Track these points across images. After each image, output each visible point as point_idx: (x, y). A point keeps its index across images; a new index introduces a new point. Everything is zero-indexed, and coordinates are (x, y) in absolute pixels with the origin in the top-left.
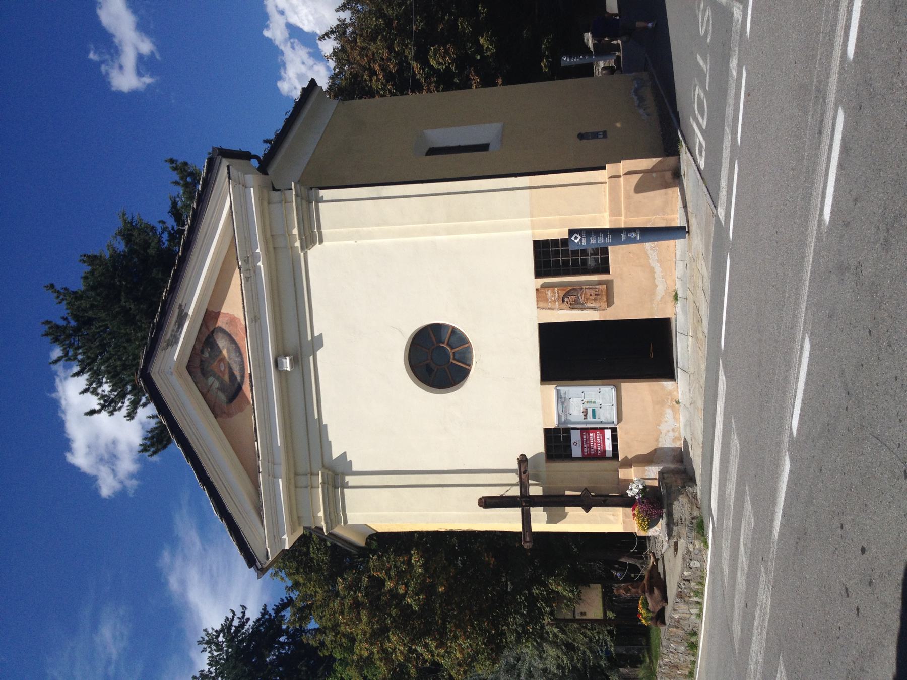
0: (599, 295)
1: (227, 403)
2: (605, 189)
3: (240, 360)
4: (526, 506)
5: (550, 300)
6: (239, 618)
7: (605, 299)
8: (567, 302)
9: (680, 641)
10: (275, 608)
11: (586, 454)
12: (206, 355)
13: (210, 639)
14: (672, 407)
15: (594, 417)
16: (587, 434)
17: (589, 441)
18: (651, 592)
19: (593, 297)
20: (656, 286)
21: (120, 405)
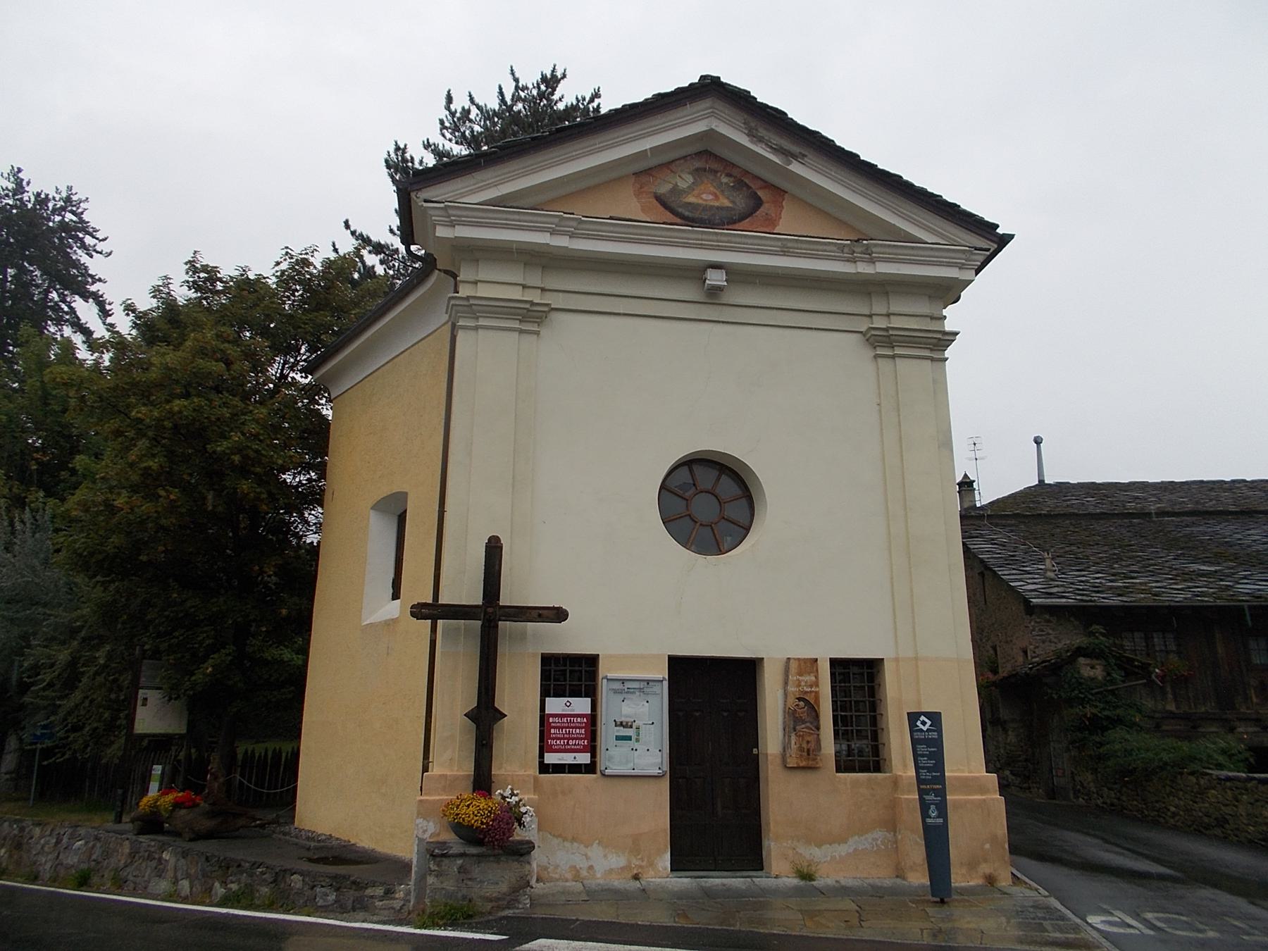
0: (808, 754)
1: (655, 193)
3: (717, 221)
4: (486, 613)
5: (801, 678)
6: (95, 246)
7: (801, 765)
8: (797, 705)
9: (94, 857)
10: (100, 293)
11: (551, 720)
12: (725, 180)
13: (71, 202)
16: (584, 725)
17: (573, 728)
18: (211, 815)
19: (805, 745)
21: (448, 136)
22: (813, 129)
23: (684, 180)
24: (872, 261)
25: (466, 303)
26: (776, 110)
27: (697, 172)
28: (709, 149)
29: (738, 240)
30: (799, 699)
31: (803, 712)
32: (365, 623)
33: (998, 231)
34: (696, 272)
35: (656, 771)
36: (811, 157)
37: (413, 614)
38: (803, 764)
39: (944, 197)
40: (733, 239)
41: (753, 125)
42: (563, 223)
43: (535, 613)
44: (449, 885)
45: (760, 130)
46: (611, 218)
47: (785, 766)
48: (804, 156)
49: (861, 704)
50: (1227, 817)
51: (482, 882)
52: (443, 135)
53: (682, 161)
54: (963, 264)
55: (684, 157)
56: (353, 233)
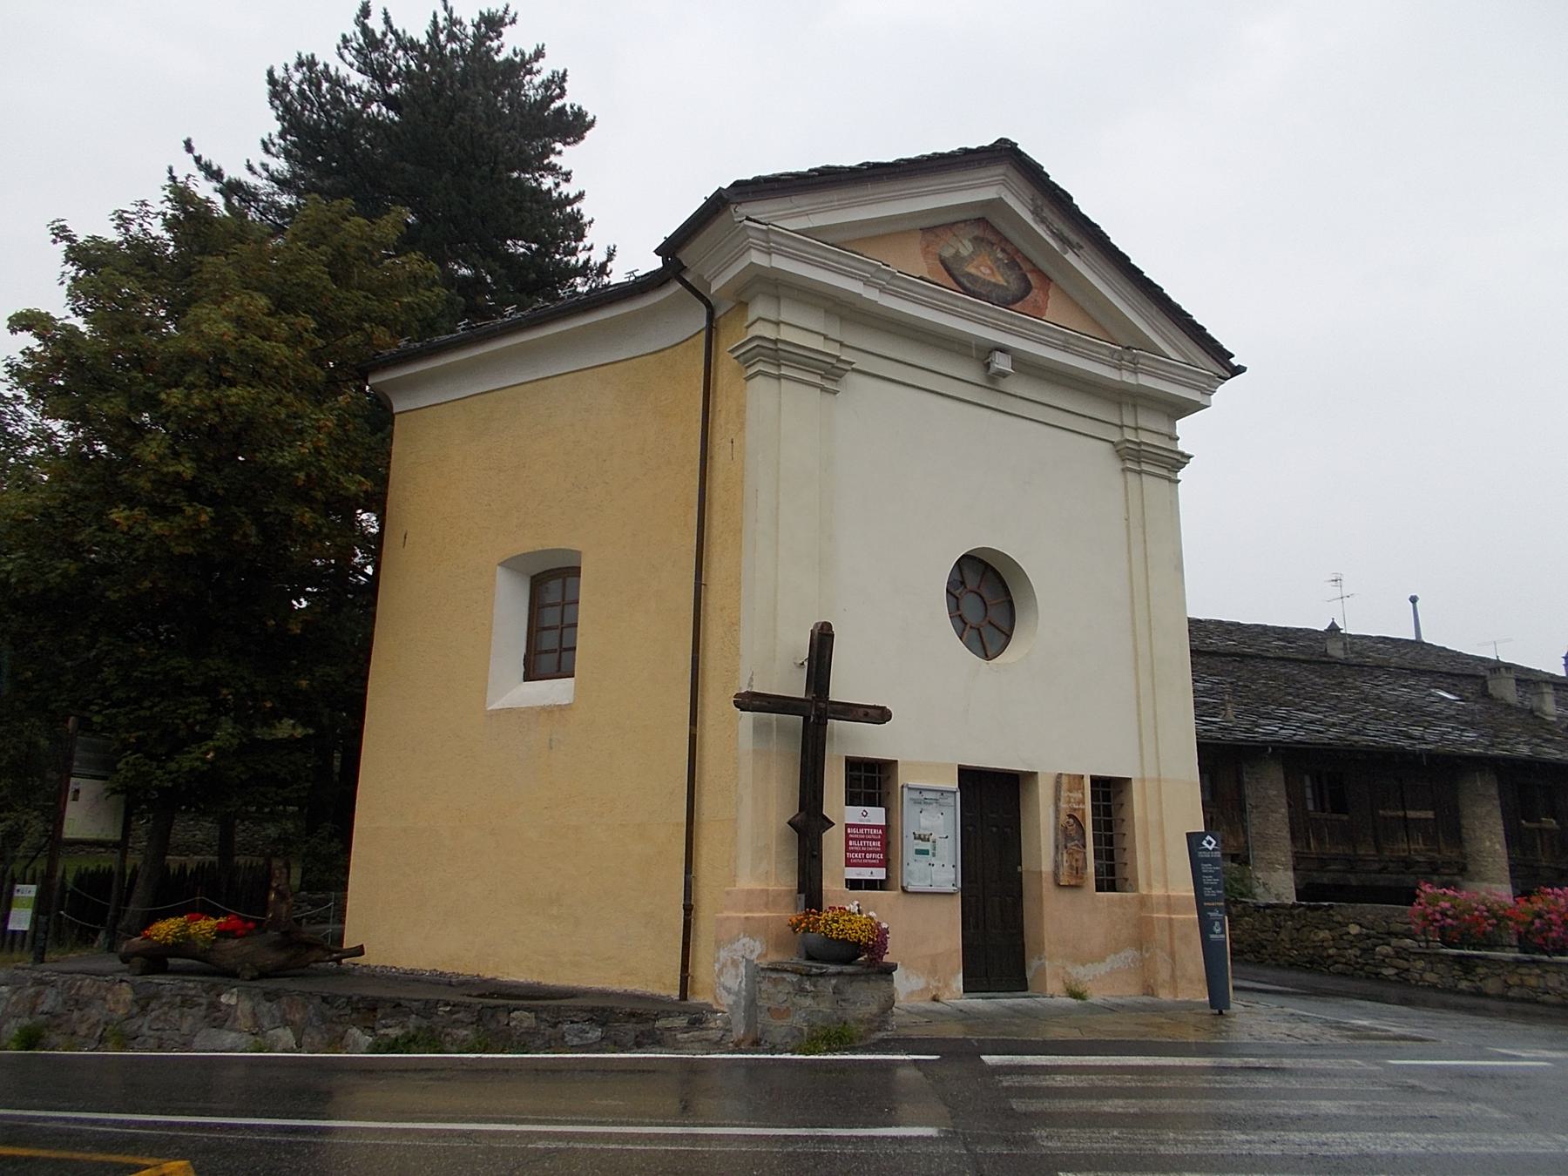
2: (1188, 891)
12: (1000, 255)
14: (926, 989)
15: (919, 852)
17: (869, 840)
19: (1074, 863)
20: (1083, 965)
21: (350, 58)
22: (1095, 222)
23: (966, 249)
24: (1135, 372)
25: (771, 346)
26: (1065, 192)
27: (977, 241)
28: (987, 218)
29: (1029, 326)
30: (1070, 816)
31: (1072, 830)
32: (496, 706)
33: (1231, 360)
34: (984, 353)
35: (951, 889)
36: (1088, 250)
37: (737, 704)
38: (1073, 883)
39: (1194, 318)
40: (1025, 325)
41: (1039, 203)
42: (877, 274)
43: (861, 712)
44: (825, 1007)
45: (1045, 210)
46: (920, 278)
47: (1059, 885)
48: (1082, 247)
49: (849, 830)
50: (1265, 943)
51: (855, 1003)
52: (342, 57)
53: (963, 225)
54: (1205, 389)
55: (965, 221)
56: (198, 159)
